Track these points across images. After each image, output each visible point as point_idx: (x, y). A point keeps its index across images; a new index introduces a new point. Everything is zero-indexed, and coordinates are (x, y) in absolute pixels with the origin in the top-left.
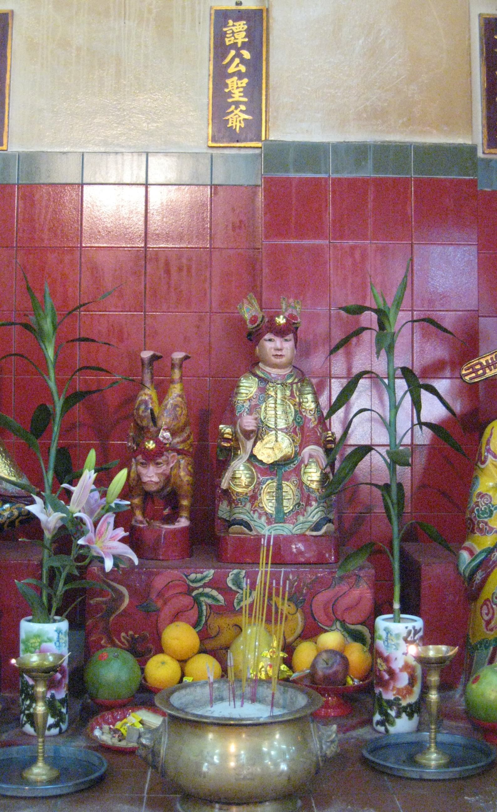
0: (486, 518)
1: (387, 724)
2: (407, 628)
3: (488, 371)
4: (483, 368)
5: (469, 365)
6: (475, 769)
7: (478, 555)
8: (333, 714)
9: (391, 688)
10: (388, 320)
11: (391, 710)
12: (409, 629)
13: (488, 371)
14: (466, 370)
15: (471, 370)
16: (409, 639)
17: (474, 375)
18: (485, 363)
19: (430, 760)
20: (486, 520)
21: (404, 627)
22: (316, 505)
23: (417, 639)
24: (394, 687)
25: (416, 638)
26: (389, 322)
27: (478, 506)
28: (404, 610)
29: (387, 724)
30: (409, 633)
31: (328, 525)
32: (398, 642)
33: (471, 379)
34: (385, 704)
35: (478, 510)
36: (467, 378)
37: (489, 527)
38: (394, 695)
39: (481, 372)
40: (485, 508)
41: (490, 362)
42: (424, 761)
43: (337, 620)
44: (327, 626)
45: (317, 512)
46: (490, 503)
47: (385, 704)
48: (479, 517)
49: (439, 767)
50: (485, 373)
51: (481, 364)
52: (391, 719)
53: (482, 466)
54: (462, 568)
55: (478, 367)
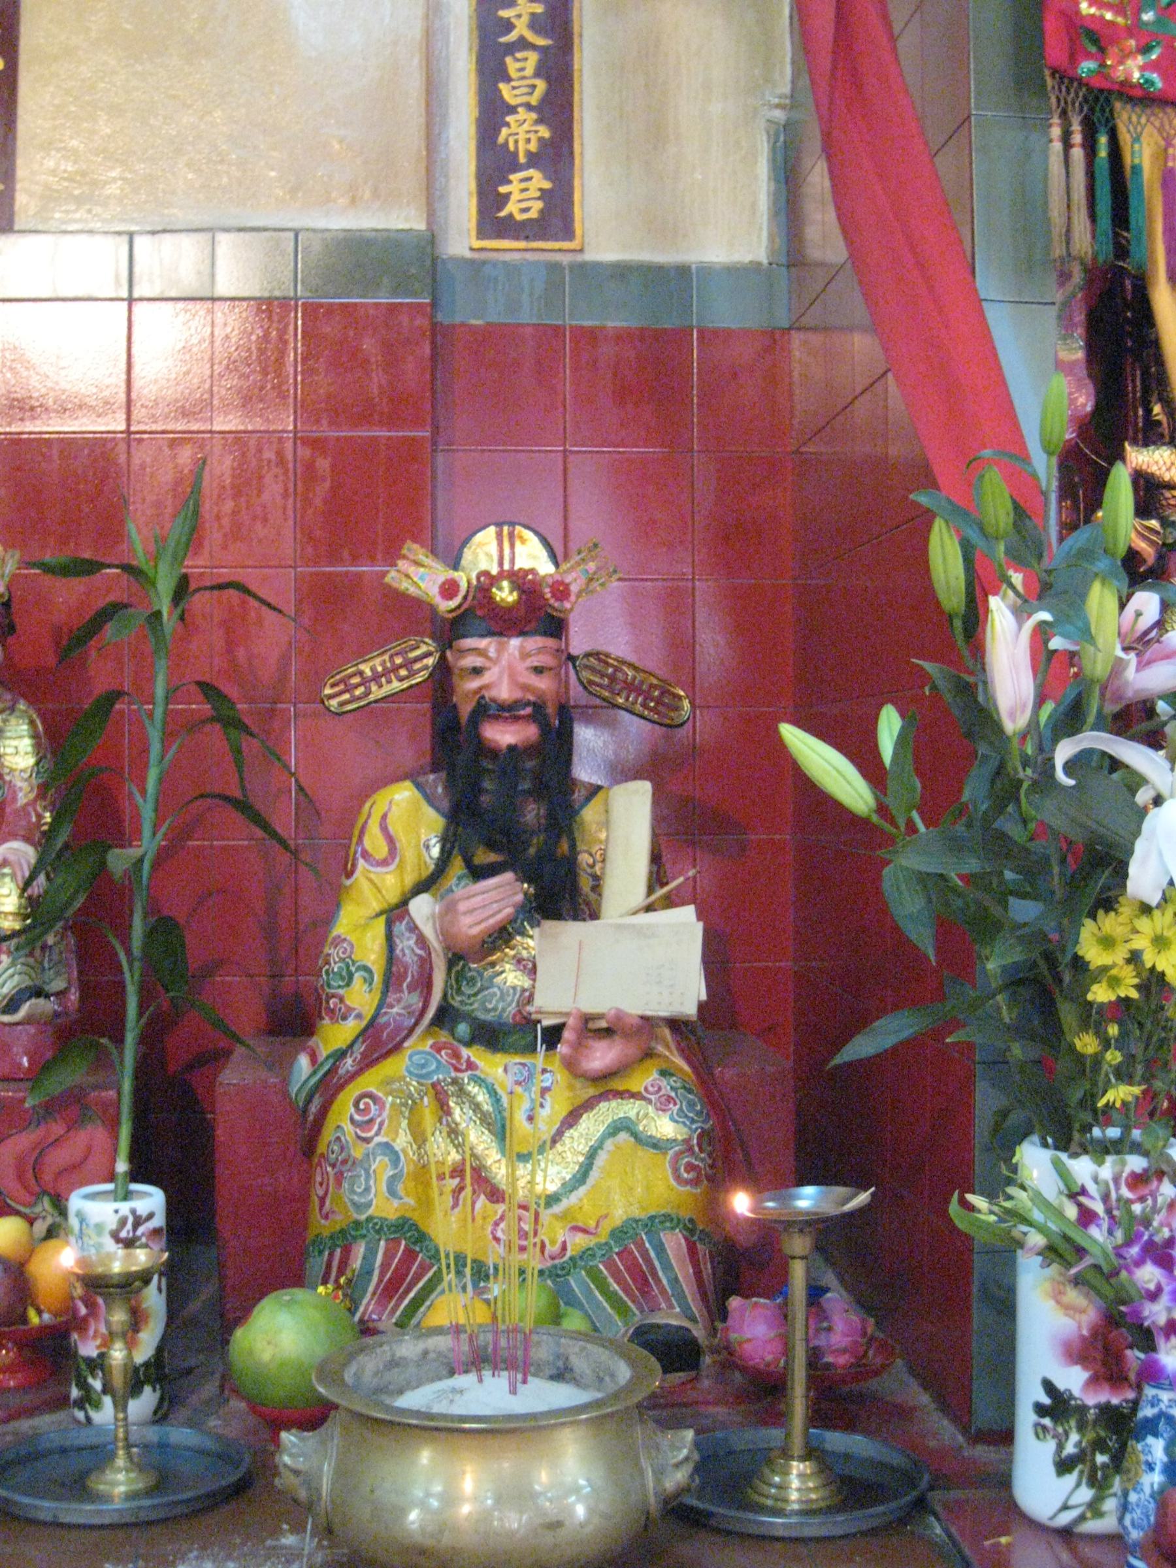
0: (340, 987)
1: (87, 1406)
2: (116, 1211)
3: (374, 688)
4: (365, 682)
5: (338, 677)
6: (154, 1507)
7: (322, 1064)
8: (12, 1383)
9: (91, 1332)
10: (156, 588)
11: (94, 1377)
12: (121, 1213)
13: (374, 688)
14: (333, 686)
15: (342, 687)
16: (123, 1234)
17: (347, 696)
18: (368, 673)
19: (115, 1484)
20: (341, 991)
21: (111, 1212)
22: (10, 960)
23: (143, 1234)
24: (96, 1332)
25: (140, 1231)
26: (157, 594)
27: (328, 963)
28: (137, 1175)
29: (87, 1406)
30: (123, 1222)
31: (33, 1000)
32: (100, 1240)
33: (342, 704)
34: (83, 1366)
35: (327, 972)
36: (333, 703)
37: (346, 1006)
38: (98, 1347)
39: (359, 692)
40: (339, 968)
41: (380, 669)
42: (102, 1487)
43: (45, 1192)
44: (24, 1205)
45: (12, 976)
46: (350, 957)
47: (83, 1366)
48: (329, 986)
49: (131, 1496)
50: (368, 693)
51: (361, 673)
52: (94, 1396)
53: (348, 883)
54: (293, 1090)
55: (356, 680)
